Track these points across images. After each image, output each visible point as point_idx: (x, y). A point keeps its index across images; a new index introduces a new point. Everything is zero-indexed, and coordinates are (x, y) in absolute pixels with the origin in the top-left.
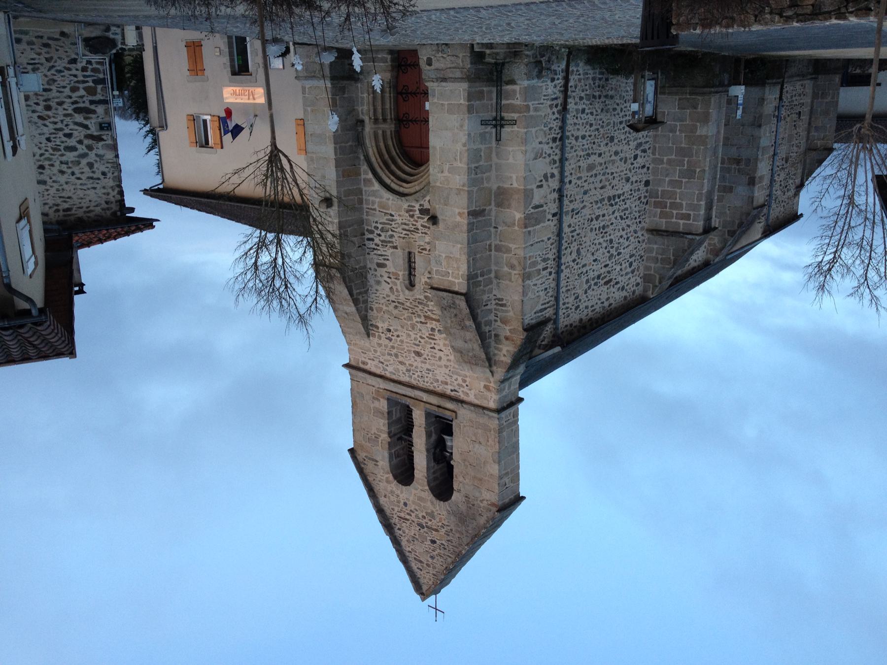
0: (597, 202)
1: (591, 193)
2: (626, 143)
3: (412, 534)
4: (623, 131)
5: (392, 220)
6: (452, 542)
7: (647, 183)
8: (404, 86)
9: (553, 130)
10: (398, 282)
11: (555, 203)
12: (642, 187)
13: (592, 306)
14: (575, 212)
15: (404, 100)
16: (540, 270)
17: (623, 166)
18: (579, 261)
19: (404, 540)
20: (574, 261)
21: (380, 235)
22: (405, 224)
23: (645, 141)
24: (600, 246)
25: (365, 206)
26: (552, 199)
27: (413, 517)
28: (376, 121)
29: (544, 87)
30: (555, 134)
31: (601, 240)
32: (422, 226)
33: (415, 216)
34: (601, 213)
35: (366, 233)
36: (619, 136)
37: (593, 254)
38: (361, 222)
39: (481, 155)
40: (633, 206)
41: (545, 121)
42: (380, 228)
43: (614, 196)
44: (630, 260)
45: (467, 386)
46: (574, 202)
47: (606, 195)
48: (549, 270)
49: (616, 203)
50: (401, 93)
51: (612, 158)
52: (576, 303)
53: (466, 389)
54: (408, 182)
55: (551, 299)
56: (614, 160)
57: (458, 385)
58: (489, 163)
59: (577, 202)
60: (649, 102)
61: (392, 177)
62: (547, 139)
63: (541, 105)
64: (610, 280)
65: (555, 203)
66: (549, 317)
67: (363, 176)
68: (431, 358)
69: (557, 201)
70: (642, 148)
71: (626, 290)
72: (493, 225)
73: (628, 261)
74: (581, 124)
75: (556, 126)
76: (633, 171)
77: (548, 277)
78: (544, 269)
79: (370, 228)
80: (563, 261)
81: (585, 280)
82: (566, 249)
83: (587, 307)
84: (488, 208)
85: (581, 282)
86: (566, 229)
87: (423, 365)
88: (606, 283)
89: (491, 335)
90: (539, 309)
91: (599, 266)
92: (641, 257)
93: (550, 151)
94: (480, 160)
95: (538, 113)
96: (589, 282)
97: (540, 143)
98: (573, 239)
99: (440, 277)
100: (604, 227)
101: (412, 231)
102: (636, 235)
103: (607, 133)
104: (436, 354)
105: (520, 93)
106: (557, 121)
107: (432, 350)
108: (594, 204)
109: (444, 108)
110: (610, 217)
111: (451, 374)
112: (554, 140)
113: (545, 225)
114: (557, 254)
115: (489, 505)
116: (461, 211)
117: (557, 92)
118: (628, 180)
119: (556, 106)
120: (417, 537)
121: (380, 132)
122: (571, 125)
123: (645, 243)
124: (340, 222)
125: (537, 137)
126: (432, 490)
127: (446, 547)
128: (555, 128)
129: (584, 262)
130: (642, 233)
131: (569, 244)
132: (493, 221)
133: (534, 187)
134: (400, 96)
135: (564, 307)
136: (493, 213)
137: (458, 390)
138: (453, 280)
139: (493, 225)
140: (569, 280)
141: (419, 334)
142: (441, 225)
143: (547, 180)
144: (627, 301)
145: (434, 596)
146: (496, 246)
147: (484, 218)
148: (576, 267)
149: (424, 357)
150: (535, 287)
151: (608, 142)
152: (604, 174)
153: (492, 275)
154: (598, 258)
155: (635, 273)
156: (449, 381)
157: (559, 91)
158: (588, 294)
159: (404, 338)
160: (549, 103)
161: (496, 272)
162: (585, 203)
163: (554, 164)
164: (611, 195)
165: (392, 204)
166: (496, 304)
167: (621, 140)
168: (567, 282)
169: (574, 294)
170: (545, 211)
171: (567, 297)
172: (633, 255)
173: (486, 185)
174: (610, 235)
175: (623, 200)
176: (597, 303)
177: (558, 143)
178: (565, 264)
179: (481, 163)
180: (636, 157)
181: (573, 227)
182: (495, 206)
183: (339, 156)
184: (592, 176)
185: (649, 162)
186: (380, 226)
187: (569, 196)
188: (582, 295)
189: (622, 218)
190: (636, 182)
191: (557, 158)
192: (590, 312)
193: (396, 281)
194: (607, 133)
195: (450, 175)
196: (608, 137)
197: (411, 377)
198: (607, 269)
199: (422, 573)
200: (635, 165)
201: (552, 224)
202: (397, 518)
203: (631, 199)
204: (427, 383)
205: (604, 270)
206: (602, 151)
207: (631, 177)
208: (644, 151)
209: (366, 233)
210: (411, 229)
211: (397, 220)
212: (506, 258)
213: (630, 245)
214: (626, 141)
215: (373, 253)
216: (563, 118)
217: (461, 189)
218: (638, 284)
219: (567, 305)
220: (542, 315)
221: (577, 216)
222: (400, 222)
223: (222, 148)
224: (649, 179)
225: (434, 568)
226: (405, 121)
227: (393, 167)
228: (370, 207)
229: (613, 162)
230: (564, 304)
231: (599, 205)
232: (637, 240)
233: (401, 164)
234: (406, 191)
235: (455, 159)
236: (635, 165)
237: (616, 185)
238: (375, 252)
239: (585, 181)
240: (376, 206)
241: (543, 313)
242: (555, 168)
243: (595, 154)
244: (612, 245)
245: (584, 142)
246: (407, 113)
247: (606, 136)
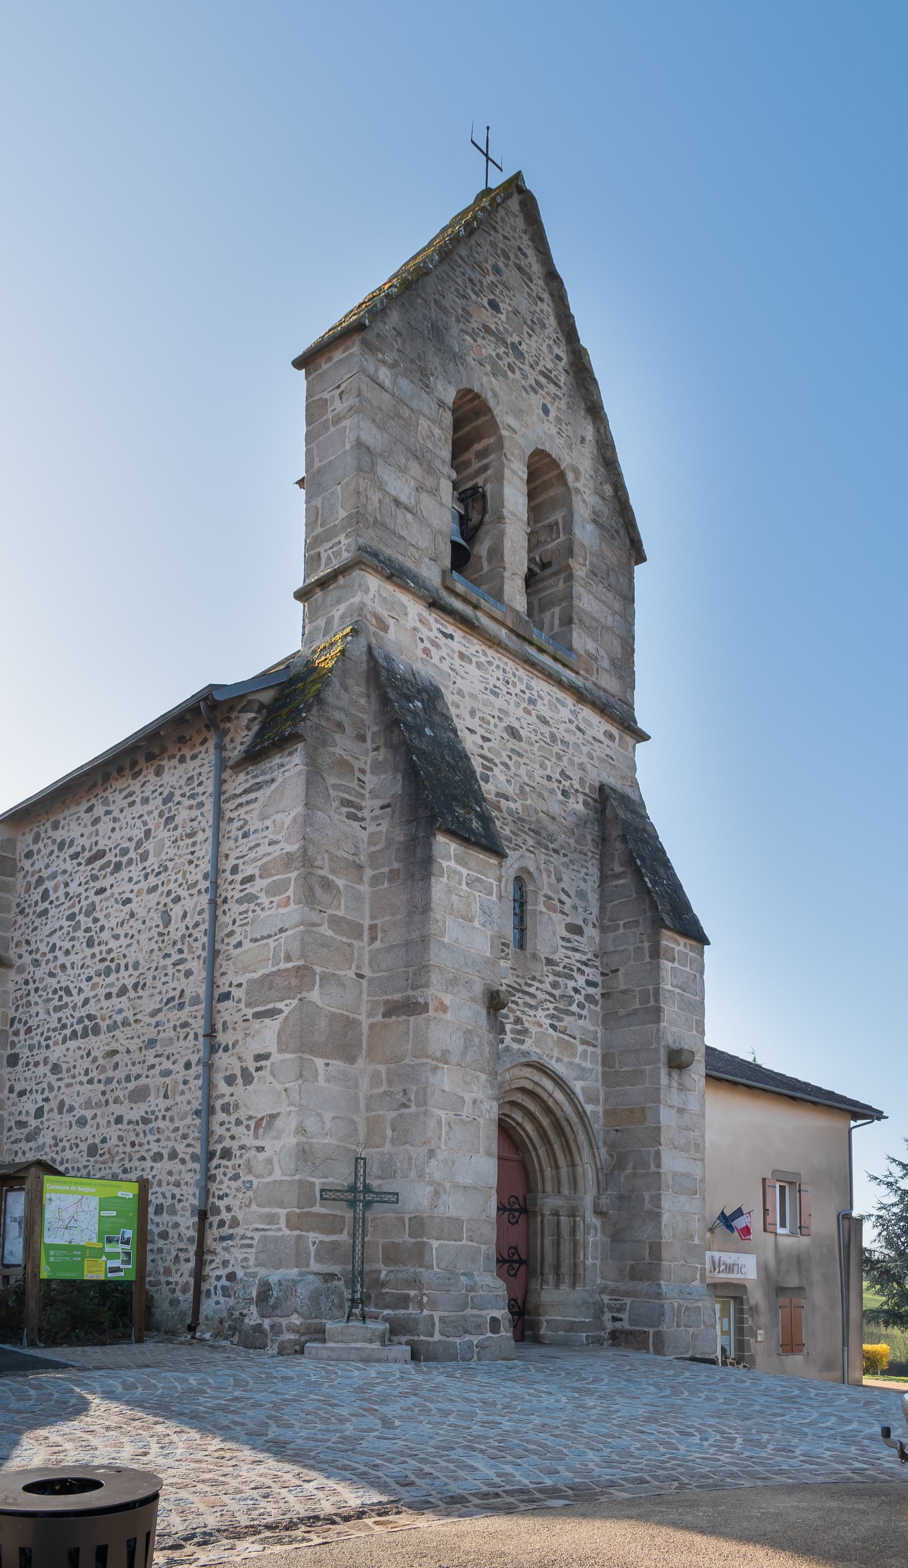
0: (125, 1023)
1: (139, 1041)
2: (61, 1140)
3: (534, 338)
4: (69, 1165)
5: (552, 1017)
6: (457, 290)
7: (13, 1060)
8: (515, 1275)
9: (229, 1175)
10: (546, 890)
11: (225, 1023)
12: (24, 1053)
13: (132, 804)
14: (177, 1002)
15: (515, 1248)
16: (261, 877)
17: (69, 1098)
18: (164, 900)
19: (551, 330)
20: (177, 899)
21: (576, 990)
22: (531, 1006)
23: (20, 1145)
24: (116, 931)
25: (598, 1051)
26: (230, 1031)
27: (533, 376)
28: (573, 1213)
29: (251, 1262)
30: (227, 1167)
31: (113, 944)
33: (512, 1019)
34: (115, 1000)
35: (598, 997)
36: (78, 1156)
37: (132, 915)
38: (609, 1019)
39: (394, 1130)
40: (42, 1015)
41: (250, 1193)
42: (575, 1005)
43: (85, 1035)
44: (46, 904)
45: (422, 640)
46: (178, 1024)
47: (104, 1037)
48: (239, 877)
49: (81, 1020)
50: (521, 1262)
51: (93, 1112)
52: (170, 810)
53: (424, 633)
54: (523, 1090)
55: (233, 815)
56: (86, 1109)
57: (438, 647)
58: (374, 1113)
59: (171, 1024)
60: (15, 1220)
61: (550, 1102)
62: (245, 1157)
63: (260, 1226)
64: (90, 861)
65: (225, 1023)
66: (237, 774)
67: (600, 1109)
68: (490, 718)
69: (219, 1026)
70: (26, 1131)
71: (54, 842)
72: (365, 983)
73: (51, 902)
74: (164, 1184)
75: (222, 1182)
76: (45, 1085)
77: (241, 861)
78: (250, 879)
79: (593, 1007)
80: (205, 899)
81: (151, 859)
82: (197, 925)
83: (145, 801)
84: (379, 1018)
85: (160, 854)
86: (197, 967)
87: (505, 706)
88: (101, 854)
89: (373, 742)
90: (262, 791)
91: (116, 890)
92: (22, 912)
93: (235, 1130)
94: (394, 1120)
95: (268, 1210)
96: (141, 855)
97: (261, 1149)
98: (179, 946)
99: (483, 878)
100: (108, 972)
101: (518, 991)
102: (34, 956)
103: (104, 1163)
104: (481, 726)
105: (309, 1254)
106: (221, 1193)
107: (487, 735)
108: (132, 1019)
109: (470, 1233)
110: (93, 993)
111: (452, 673)
112: (227, 1154)
113: (249, 976)
114: (219, 912)
115: (380, 351)
116: (441, 1015)
117: (222, 1253)
118: (56, 1069)
119: (222, 1224)
120: (526, 328)
121: (565, 1190)
122: (186, 1183)
123: (15, 940)
124: (658, 1020)
125: (269, 1161)
126: (493, 426)
127: (469, 285)
128: (226, 1179)
129: (154, 897)
130: (20, 962)
131: (190, 936)
132: (365, 991)
133: (276, 1057)
134: (523, 1257)
135: (200, 799)
136: (364, 1008)
137: (440, 636)
138: (460, 868)
139: (365, 983)
140: (190, 857)
141: (511, 773)
142: (478, 988)
143: (244, 1070)
144: (52, 819)
145: (493, 185)
146: (360, 937)
147: (389, 997)
148: (172, 886)
149: (504, 725)
150: (275, 838)
151: (100, 1146)
152: (109, 1081)
153: (368, 873)
154: (120, 906)
155: (36, 877)
156: (457, 662)
157: (216, 1254)
158: (143, 829)
159: (538, 773)
160: (239, 1231)
161: (361, 880)
162: (153, 1021)
163: (228, 1104)
164: (92, 1038)
165: (552, 1050)
166: (360, 808)
167: (71, 1148)
168: (192, 853)
169: (175, 828)
170: (249, 1005)
171: (192, 820)
172: (40, 915)
173: (382, 1068)
174: (93, 956)
175: (64, 1027)
176: (122, 811)
177: (218, 1148)
178: (200, 892)
179: (393, 1114)
180: (39, 1113)
181: (179, 971)
182: (360, 1024)
183: (652, 1150)
184: (138, 1077)
185: (10, 1102)
187: (191, 1036)
188: (157, 826)
189: (68, 992)
190: (37, 1064)
191: (220, 1116)
192: (138, 792)
193: (550, 893)
194: (104, 1163)
195: (461, 1094)
196: (101, 1155)
197: (529, 687)
198: (98, 885)
199: (518, 243)
200: (40, 1097)
201: (231, 977)
202: (562, 384)
203: (49, 1030)
204: (498, 667)
205: (106, 883)
206: (115, 1127)
207: (49, 1074)
208: (21, 1124)
209: (598, 997)
210: (520, 995)
211: (546, 1016)
212: (338, 907)
213: (47, 936)
214: (61, 1145)
215: (589, 956)
216: (208, 1198)
217: (441, 1061)
218: (29, 855)
219: (193, 802)
220: (255, 777)
221: (169, 995)
222: (540, 1013)
223: (764, 1180)
224: (10, 1069)
225: (493, 245)
226: (516, 1210)
227: (545, 1122)
228: (590, 1049)
229: (88, 1104)
230: (202, 804)
231: (119, 1018)
232: (33, 947)
233: (529, 1127)
234: (527, 1072)
235: (450, 1127)
236: (40, 1097)
237: (82, 1057)
238: (584, 958)
239: (152, 1067)
240: (580, 1048)
241: (252, 782)
242: (223, 1096)
243: (129, 1123)
244: (88, 935)
245: (155, 1147)
246: (513, 1224)
247: (107, 1156)
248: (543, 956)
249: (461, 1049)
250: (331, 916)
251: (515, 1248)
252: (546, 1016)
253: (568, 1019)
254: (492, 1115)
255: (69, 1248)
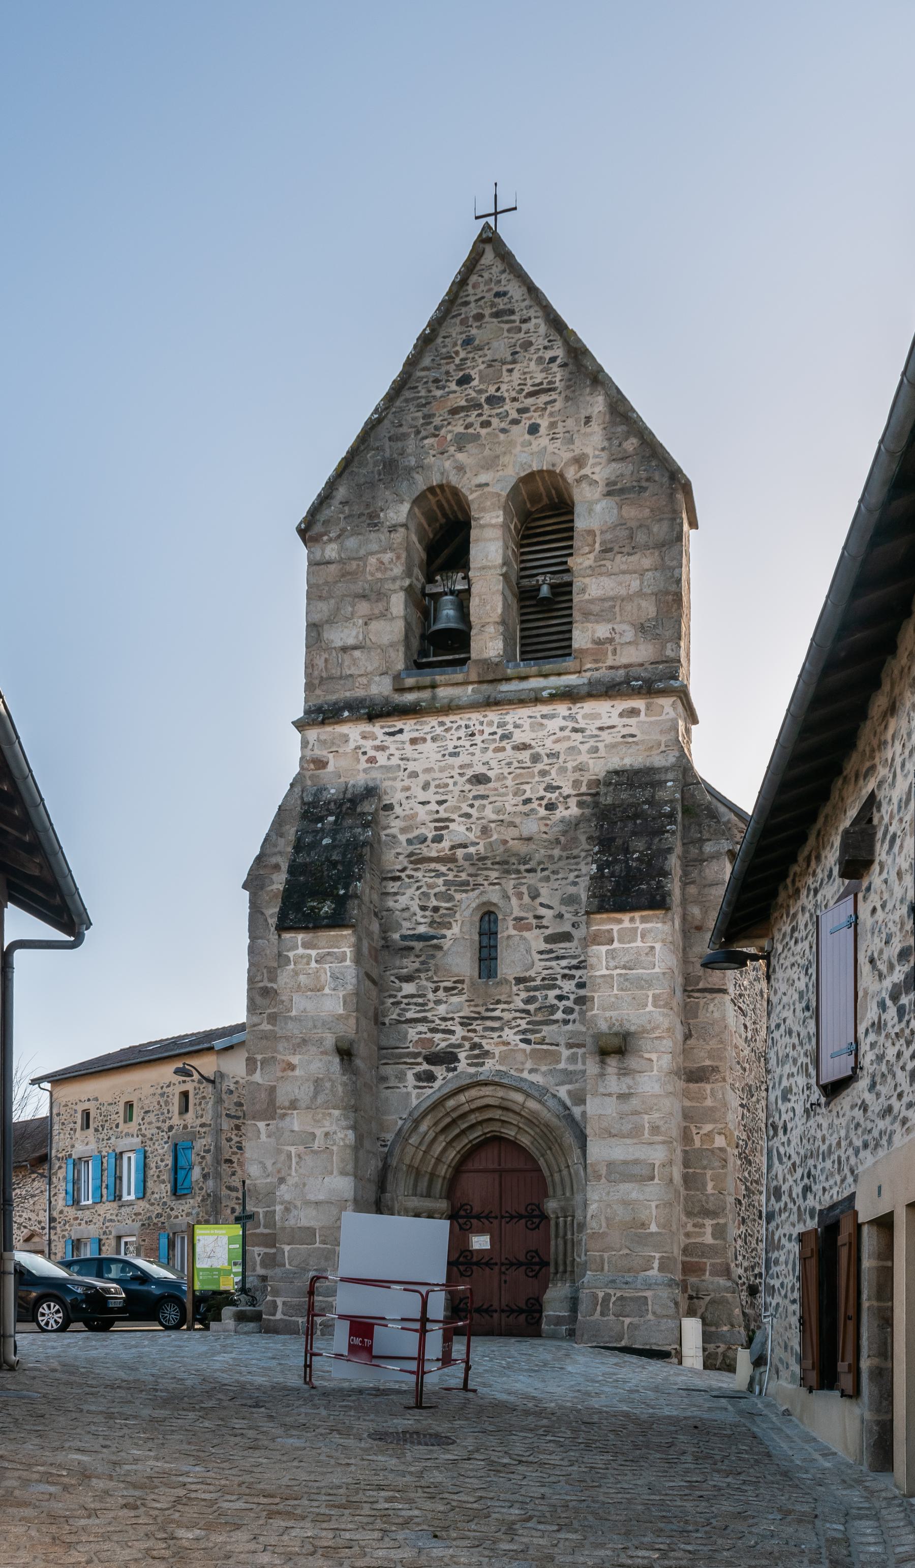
5: (524, 1032)
10: (517, 913)
15: (536, 1252)
21: (560, 998)
22: (493, 1029)
32: (452, 1032)
101: (476, 1019)
105: (255, 1263)
186: (559, 1015)
248: (511, 978)
249: (311, 1094)
250: (269, 1014)
251: (536, 1252)
252: (515, 1034)
253: (546, 1030)
254: (347, 1142)
255: (211, 1270)
